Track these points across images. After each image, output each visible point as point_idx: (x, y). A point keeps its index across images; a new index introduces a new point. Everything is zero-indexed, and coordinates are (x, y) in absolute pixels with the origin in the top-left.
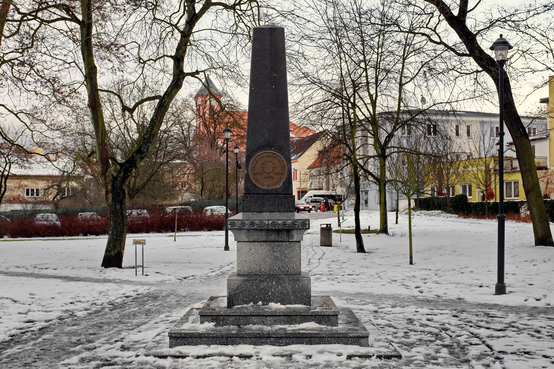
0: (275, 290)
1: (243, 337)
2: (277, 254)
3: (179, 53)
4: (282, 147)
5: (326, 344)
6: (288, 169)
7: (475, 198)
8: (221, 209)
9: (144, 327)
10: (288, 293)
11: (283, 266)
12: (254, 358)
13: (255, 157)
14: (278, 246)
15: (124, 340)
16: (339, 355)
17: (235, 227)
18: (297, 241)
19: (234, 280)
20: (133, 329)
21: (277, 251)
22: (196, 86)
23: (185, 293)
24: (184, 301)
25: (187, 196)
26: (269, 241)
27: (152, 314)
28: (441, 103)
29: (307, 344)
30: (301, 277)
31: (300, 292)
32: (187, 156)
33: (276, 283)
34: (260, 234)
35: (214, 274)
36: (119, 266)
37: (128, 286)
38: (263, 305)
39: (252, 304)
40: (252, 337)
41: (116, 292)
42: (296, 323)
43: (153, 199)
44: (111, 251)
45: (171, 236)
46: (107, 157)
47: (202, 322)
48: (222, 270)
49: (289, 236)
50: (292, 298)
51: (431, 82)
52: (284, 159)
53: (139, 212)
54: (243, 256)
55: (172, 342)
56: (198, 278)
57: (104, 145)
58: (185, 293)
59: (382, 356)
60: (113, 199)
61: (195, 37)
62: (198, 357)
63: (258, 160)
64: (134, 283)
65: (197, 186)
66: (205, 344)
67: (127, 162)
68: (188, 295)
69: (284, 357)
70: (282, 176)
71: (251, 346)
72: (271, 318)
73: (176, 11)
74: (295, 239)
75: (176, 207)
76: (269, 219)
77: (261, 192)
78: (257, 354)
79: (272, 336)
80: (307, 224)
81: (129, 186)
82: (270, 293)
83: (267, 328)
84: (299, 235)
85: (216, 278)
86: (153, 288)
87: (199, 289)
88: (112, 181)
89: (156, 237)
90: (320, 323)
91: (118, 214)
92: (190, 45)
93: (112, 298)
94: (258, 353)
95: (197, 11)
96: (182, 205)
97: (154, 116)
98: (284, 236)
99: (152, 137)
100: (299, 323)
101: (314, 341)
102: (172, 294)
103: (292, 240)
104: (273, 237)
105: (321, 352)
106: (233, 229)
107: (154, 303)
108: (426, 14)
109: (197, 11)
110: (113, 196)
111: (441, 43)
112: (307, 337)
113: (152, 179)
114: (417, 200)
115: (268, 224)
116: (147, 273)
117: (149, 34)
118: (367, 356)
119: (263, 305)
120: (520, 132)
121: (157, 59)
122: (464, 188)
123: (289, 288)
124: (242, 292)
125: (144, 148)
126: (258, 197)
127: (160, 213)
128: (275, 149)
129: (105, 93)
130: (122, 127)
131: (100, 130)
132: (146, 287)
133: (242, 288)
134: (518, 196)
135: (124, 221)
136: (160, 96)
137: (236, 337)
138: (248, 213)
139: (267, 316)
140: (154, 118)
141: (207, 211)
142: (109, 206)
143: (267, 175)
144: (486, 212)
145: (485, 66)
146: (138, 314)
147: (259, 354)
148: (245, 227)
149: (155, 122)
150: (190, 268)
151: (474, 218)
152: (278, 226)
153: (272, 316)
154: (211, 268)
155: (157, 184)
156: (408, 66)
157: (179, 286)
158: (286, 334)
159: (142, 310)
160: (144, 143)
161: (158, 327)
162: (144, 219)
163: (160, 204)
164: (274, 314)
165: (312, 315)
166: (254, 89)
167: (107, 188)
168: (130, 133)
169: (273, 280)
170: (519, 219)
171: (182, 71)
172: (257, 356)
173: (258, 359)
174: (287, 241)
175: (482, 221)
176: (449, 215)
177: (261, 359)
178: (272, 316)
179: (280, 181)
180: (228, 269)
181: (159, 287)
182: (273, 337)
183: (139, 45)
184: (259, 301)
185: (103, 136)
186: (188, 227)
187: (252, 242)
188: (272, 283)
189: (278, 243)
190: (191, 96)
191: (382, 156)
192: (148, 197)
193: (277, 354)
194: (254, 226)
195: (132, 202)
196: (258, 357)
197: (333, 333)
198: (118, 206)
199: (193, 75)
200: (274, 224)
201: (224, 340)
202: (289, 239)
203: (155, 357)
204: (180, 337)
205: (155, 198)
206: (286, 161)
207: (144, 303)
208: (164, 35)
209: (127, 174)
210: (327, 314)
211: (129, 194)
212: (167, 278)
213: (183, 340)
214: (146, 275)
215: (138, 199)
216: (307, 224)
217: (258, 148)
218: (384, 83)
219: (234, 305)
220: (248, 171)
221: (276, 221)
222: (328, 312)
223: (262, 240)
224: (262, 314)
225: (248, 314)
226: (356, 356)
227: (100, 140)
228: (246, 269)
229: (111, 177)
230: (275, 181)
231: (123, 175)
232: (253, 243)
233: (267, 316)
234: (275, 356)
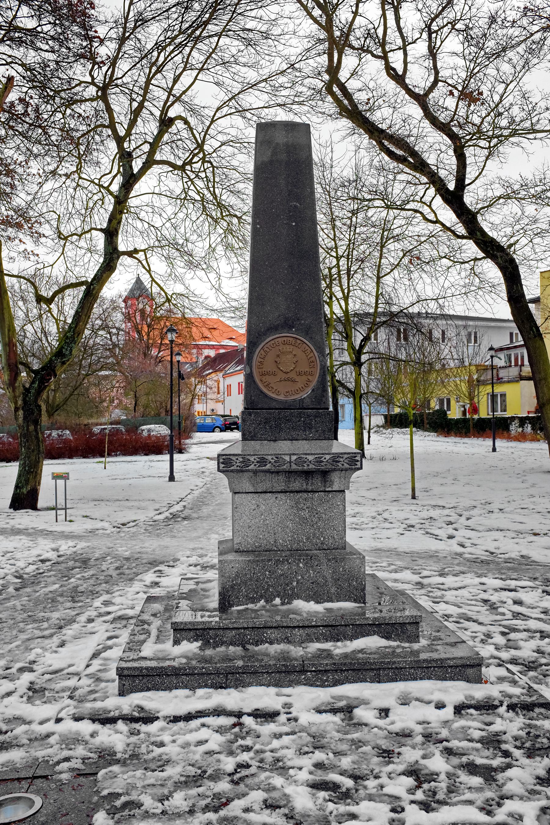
0: (303, 577)
1: (255, 673)
2: (305, 514)
3: (112, 224)
4: (310, 327)
5: (407, 680)
6: (321, 365)
7: (455, 413)
8: (160, 429)
9: (69, 632)
10: (326, 581)
11: (314, 534)
12: (283, 718)
13: (263, 344)
14: (305, 499)
15: (35, 667)
16: (440, 706)
17: (232, 468)
18: (338, 491)
19: (231, 561)
20: (51, 636)
21: (305, 508)
22: (133, 270)
23: (127, 553)
24: (128, 568)
25: (117, 414)
26: (291, 492)
27: (82, 598)
28: (426, 300)
29: (372, 682)
30: (347, 554)
31: (348, 580)
32: (116, 366)
33: (305, 564)
34: (275, 478)
35: (161, 517)
36: (34, 507)
37: (46, 542)
38: (283, 604)
39: (262, 602)
40: (272, 672)
41: (28, 552)
42: (345, 638)
43: (77, 417)
44: (23, 487)
45: (100, 462)
46: (16, 362)
47: (177, 642)
48: (171, 510)
49: (325, 482)
50: (333, 590)
51: (415, 275)
52: (313, 348)
53: (60, 433)
54: (245, 518)
55: (124, 685)
56: (142, 523)
57: (11, 345)
58: (127, 553)
59: (516, 704)
60: (25, 418)
61: (132, 202)
62: (176, 719)
63: (268, 350)
64: (54, 535)
65: (129, 402)
66: (186, 687)
67: (43, 369)
68: (133, 557)
69: (338, 714)
70: (310, 378)
71: (273, 690)
72: (301, 631)
73: (108, 171)
74: (336, 487)
75: (106, 427)
76: (291, 452)
77: (274, 405)
78: (287, 710)
79: (310, 669)
80: (358, 461)
81: (47, 402)
82: (295, 584)
83: (297, 651)
84: (342, 479)
85: (166, 524)
86: (82, 544)
87: (146, 545)
88: (23, 394)
89: (81, 463)
90: (388, 638)
91: (31, 437)
92: (127, 213)
93: (21, 564)
94: (288, 706)
95: (136, 170)
96: (111, 424)
97: (78, 308)
98: (317, 483)
99: (76, 335)
100: (352, 638)
101: (386, 675)
102: (108, 555)
103: (330, 489)
104: (297, 484)
105: (405, 701)
106: (227, 471)
107: (83, 574)
108: (421, 184)
109: (136, 170)
110: (24, 414)
111: (437, 222)
112: (373, 669)
113: (76, 393)
114: (389, 417)
115: (290, 462)
116: (72, 518)
117: (71, 205)
118: (489, 706)
119: (283, 604)
120: (533, 332)
121: (82, 234)
122: (441, 401)
123: (328, 573)
124: (245, 583)
125: (67, 350)
126: (270, 414)
127: (86, 435)
128: (297, 332)
129: (14, 280)
130: (39, 330)
131: (7, 326)
132: (71, 543)
133: (246, 574)
134: (505, 411)
135: (39, 447)
136: (87, 281)
137: (243, 673)
138: (253, 442)
139: (294, 627)
140: (80, 310)
141: (143, 430)
142: (19, 427)
143: (284, 376)
144: (471, 430)
145: (489, 251)
146: (59, 599)
147: (291, 710)
148: (250, 468)
149: (80, 316)
150: (130, 508)
151: (456, 436)
152: (308, 465)
153: (303, 627)
154: (157, 508)
155: (81, 399)
156: (386, 255)
157: (117, 540)
158: (334, 664)
159: (65, 588)
160: (66, 343)
161: (94, 630)
162: (67, 441)
163: (86, 422)
164: (307, 623)
165: (374, 624)
166: (261, 227)
167: (16, 403)
168: (49, 338)
169: (299, 560)
170: (510, 438)
171: (115, 249)
172: (288, 713)
173: (289, 720)
174: (321, 491)
175: (466, 440)
176: (427, 433)
177: (296, 720)
178: (303, 627)
179: (307, 385)
180: (179, 509)
181: (89, 541)
182: (311, 671)
183: (59, 216)
184: (275, 597)
185: (11, 333)
186: (121, 451)
187: (261, 493)
188: (298, 564)
189: (305, 495)
190: (120, 296)
191: (357, 363)
192: (70, 415)
193: (323, 708)
194: (265, 466)
195: (51, 420)
196: (289, 716)
197: (419, 661)
198: (32, 428)
199: (131, 254)
200: (300, 461)
201: (221, 679)
202: (325, 486)
203: (94, 721)
204: (139, 676)
205: (79, 415)
206: (318, 352)
207: (66, 575)
208: (91, 204)
209: (44, 383)
210: (401, 620)
211: (47, 411)
212: (99, 525)
213: (145, 680)
214: (71, 521)
215: (58, 418)
216: (358, 461)
217: (268, 330)
218: (358, 276)
219: (232, 606)
220: (251, 369)
221: (305, 456)
222: (398, 616)
223: (279, 489)
224: (285, 624)
225: (260, 624)
226: (469, 707)
227: (7, 339)
228: (250, 542)
229: (22, 388)
230: (300, 385)
231: (39, 385)
232: (263, 495)
233: (294, 627)
234: (320, 712)
